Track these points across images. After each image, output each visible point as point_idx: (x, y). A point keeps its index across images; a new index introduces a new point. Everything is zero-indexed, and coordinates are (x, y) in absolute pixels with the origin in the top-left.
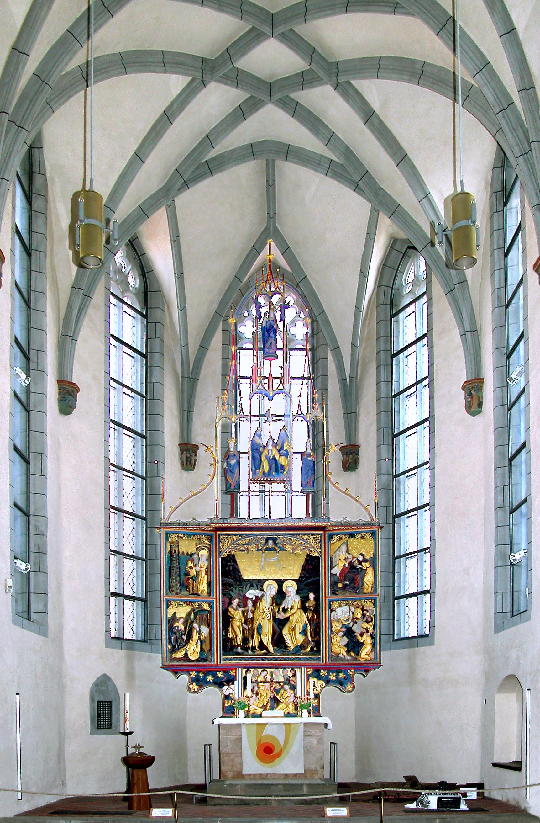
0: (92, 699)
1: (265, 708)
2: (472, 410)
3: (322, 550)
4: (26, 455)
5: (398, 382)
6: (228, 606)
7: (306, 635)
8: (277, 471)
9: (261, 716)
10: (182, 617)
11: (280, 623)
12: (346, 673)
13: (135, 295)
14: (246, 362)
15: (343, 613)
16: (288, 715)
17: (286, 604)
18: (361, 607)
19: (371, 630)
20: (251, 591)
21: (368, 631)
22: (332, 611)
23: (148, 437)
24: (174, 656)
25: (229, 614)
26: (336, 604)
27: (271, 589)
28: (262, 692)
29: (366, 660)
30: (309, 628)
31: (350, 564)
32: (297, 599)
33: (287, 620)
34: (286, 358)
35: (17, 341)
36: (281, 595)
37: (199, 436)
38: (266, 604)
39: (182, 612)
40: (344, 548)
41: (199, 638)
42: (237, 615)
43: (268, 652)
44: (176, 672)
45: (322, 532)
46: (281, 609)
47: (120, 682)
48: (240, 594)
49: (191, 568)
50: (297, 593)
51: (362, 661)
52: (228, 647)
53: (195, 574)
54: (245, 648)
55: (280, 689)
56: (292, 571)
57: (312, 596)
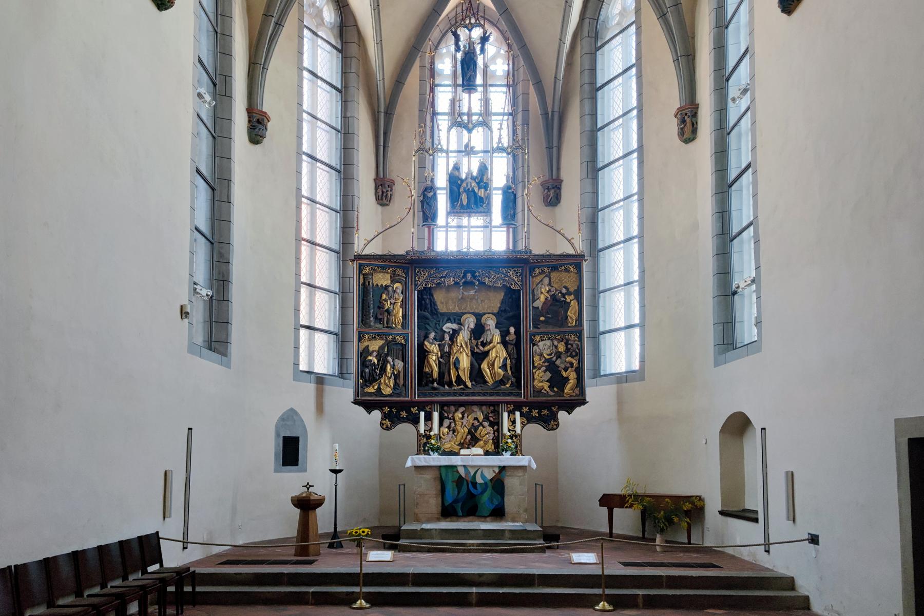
0: (277, 435)
1: (462, 445)
2: (685, 136)
4: (218, 185)
5: (603, 115)
7: (506, 370)
8: (476, 204)
9: (457, 454)
11: (478, 357)
12: (549, 410)
13: (332, 29)
14: (443, 99)
16: (487, 453)
17: (485, 338)
19: (575, 362)
20: (449, 325)
21: (572, 367)
22: (534, 345)
23: (345, 173)
24: (366, 390)
26: (538, 338)
27: (470, 322)
28: (459, 428)
30: (509, 361)
31: (553, 296)
32: (498, 332)
33: (487, 354)
34: (486, 92)
35: (200, 61)
36: (479, 331)
38: (463, 336)
39: (375, 345)
40: (546, 281)
41: (393, 373)
42: (433, 348)
43: (466, 386)
44: (369, 406)
47: (307, 413)
50: (496, 327)
51: (566, 397)
52: (424, 378)
54: (441, 382)
55: (478, 426)
56: (495, 301)
57: (512, 330)
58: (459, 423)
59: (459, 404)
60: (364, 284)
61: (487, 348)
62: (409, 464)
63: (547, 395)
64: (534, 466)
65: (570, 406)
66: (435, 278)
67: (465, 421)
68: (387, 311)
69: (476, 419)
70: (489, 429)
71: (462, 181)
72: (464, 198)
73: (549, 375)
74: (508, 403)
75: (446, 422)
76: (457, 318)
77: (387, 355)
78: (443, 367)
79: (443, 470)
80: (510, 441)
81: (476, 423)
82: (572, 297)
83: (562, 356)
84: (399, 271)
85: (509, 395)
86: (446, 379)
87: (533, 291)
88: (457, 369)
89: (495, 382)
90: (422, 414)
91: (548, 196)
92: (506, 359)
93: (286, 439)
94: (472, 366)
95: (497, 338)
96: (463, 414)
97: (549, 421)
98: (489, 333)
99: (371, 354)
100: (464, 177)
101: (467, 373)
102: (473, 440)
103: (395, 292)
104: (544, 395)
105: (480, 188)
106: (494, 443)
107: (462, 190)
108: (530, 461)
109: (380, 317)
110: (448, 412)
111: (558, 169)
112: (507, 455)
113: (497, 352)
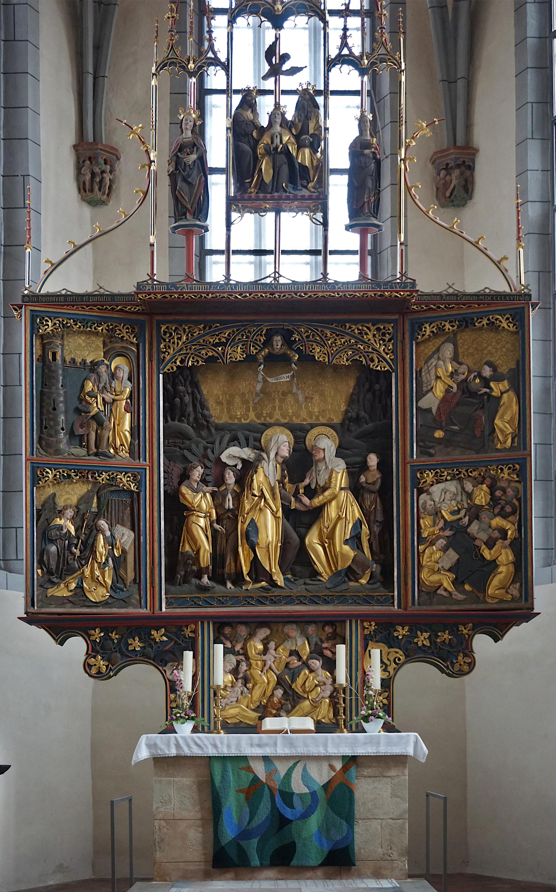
6: (180, 484)
9: (254, 729)
11: (300, 519)
12: (454, 630)
16: (320, 728)
18: (488, 481)
20: (234, 450)
24: (51, 592)
26: (429, 476)
27: (281, 443)
29: (501, 601)
30: (365, 529)
31: (464, 385)
32: (340, 466)
33: (317, 513)
36: (300, 463)
38: (267, 476)
40: (448, 350)
41: (111, 554)
43: (273, 584)
44: (60, 628)
45: (397, 317)
46: (301, 491)
48: (206, 456)
49: (92, 395)
52: (179, 566)
53: (102, 408)
56: (332, 400)
57: (373, 460)
59: (255, 623)
60: (43, 358)
61: (317, 501)
65: (499, 623)
66: (204, 345)
67: (269, 658)
73: (453, 556)
77: (97, 515)
78: (221, 541)
81: (295, 663)
82: (505, 385)
83: (484, 515)
84: (123, 332)
85: (367, 600)
86: (229, 567)
87: (419, 373)
88: (253, 547)
89: (336, 574)
91: (446, 185)
92: (358, 524)
95: (340, 479)
96: (265, 642)
97: (454, 658)
99: (61, 513)
100: (264, 121)
101: (275, 556)
103: (113, 376)
105: (300, 146)
107: (260, 150)
109: (80, 431)
111: (469, 126)
113: (339, 508)
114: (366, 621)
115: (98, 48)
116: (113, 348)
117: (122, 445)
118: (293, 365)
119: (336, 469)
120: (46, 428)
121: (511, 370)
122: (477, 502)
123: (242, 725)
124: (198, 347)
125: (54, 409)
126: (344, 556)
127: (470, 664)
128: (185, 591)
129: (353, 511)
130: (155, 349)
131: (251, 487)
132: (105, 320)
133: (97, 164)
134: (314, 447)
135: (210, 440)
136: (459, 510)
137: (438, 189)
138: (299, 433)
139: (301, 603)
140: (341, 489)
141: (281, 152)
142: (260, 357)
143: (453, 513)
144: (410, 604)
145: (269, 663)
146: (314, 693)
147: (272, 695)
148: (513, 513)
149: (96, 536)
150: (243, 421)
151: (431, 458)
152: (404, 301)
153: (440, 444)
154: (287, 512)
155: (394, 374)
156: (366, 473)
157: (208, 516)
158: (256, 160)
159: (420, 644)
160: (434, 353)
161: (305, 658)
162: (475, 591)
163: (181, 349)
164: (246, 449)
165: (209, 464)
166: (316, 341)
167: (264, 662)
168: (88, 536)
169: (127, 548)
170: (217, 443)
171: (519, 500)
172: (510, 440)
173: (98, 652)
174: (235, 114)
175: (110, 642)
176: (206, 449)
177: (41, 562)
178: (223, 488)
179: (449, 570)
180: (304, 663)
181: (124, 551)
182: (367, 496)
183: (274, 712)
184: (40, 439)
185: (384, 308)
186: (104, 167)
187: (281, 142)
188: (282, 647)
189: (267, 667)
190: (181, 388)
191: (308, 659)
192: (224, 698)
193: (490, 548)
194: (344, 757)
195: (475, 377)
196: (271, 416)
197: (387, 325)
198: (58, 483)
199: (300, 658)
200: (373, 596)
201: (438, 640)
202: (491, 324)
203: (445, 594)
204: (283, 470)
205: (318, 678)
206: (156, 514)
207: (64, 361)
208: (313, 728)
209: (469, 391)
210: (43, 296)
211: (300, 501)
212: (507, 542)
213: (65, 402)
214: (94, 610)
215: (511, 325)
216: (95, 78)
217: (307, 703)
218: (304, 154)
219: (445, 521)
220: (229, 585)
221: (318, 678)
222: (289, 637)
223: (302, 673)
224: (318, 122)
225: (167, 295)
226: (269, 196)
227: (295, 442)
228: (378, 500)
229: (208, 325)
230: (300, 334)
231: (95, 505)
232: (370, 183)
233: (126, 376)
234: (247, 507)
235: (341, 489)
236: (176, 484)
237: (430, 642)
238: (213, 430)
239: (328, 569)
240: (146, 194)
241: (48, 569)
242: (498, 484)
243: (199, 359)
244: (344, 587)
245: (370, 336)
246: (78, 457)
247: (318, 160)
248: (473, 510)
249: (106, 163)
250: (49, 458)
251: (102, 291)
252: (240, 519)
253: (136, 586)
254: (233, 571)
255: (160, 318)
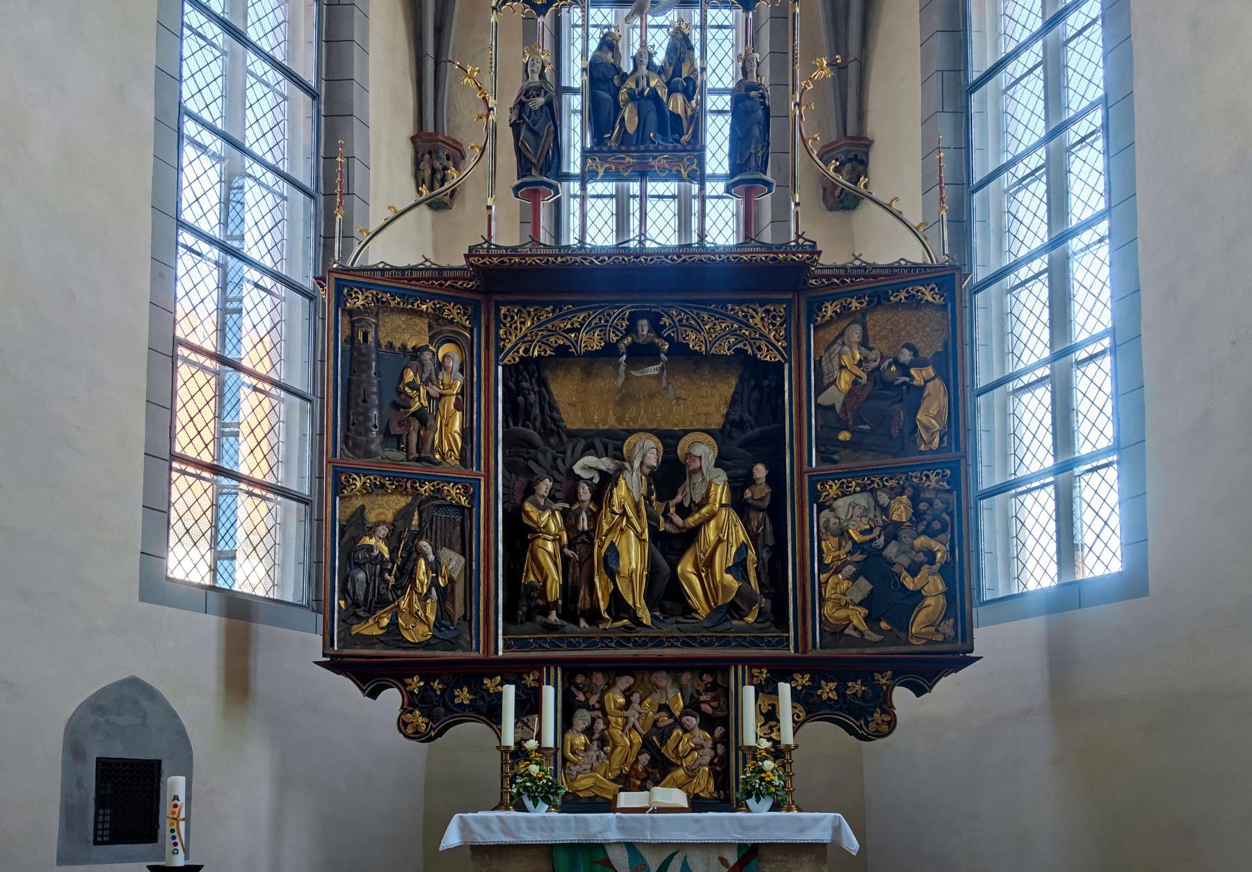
1: (627, 782)
3: (789, 344)
6: (523, 500)
9: (609, 806)
10: (384, 523)
11: (670, 545)
12: (868, 680)
15: (851, 510)
16: (697, 804)
18: (909, 491)
20: (589, 460)
23: (331, 100)
24: (356, 629)
25: (526, 521)
26: (833, 489)
27: (648, 451)
28: (617, 732)
29: (930, 642)
30: (752, 554)
31: (875, 374)
32: (721, 477)
33: (692, 536)
36: (669, 476)
37: (467, 126)
38: (629, 490)
40: (855, 333)
41: (434, 583)
42: (550, 521)
43: (637, 621)
44: (370, 676)
45: (789, 296)
46: (672, 510)
48: (555, 468)
49: (413, 386)
51: (917, 645)
52: (522, 600)
53: (426, 403)
55: (671, 728)
56: (712, 399)
57: (760, 471)
58: (616, 720)
59: (615, 669)
60: (351, 339)
61: (692, 521)
62: (452, 838)
63: (861, 641)
64: (852, 843)
65: (923, 672)
66: (553, 332)
67: (632, 715)
68: (421, 416)
69: (664, 708)
70: (701, 735)
71: (624, 77)
72: (630, 116)
73: (865, 586)
74: (754, 663)
75: (582, 718)
76: (611, 444)
77: (419, 535)
78: (575, 572)
79: (562, 859)
80: (769, 765)
81: (665, 720)
82: (930, 371)
83: (905, 534)
84: (453, 312)
85: (754, 643)
86: (583, 602)
87: (818, 363)
88: (612, 574)
89: (715, 611)
90: (509, 692)
92: (743, 548)
93: (107, 768)
94: (653, 569)
95: (720, 493)
96: (627, 694)
97: (866, 715)
98: (698, 478)
99: (371, 532)
101: (640, 587)
102: (657, 768)
103: (440, 366)
104: (852, 642)
106: (715, 774)
107: (623, 95)
108: (837, 830)
109: (396, 430)
110: (588, 691)
111: (861, 116)
112: (760, 811)
113: (719, 529)
114: (756, 667)
115: (439, 30)
116: (440, 332)
117: (451, 450)
118: (662, 356)
119: (715, 481)
120: (354, 424)
121: (937, 353)
122: (895, 517)
123: (597, 800)
124: (545, 333)
125: (365, 401)
126: (726, 588)
127: (889, 723)
128: (527, 631)
129: (737, 532)
130: (492, 336)
131: (610, 505)
132: (432, 297)
133: (438, 158)
134: (689, 455)
135: (561, 449)
136: (871, 531)
137: (824, 190)
138: (668, 440)
139: (673, 646)
140: (722, 505)
141: (648, 97)
142: (622, 347)
143: (863, 533)
144: (810, 647)
145: (632, 719)
146: (689, 758)
147: (637, 761)
148: (943, 530)
149: (416, 560)
150: (601, 427)
151: (833, 466)
152: (803, 268)
153: (845, 448)
154: (655, 535)
155: (787, 366)
156: (753, 487)
157: (557, 540)
158: (618, 109)
159: (825, 696)
160: (837, 338)
161: (677, 714)
162: (895, 630)
163: (525, 336)
164: (604, 459)
165: (559, 477)
166: (690, 326)
167: (626, 718)
168: (406, 560)
169: (455, 576)
170: (569, 452)
171: (951, 514)
172: (937, 440)
173: (415, 706)
174: (593, 57)
175: (431, 693)
176: (555, 459)
177: (344, 592)
178: (576, 506)
179: (860, 604)
180: (676, 720)
181: (451, 580)
182: (753, 514)
183: (638, 783)
184: (346, 439)
185: (775, 278)
186: (446, 163)
187: (648, 85)
188: (649, 700)
189: (629, 725)
190: (525, 384)
191: (683, 714)
192: (576, 764)
193: (914, 575)
194: (740, 846)
195: (890, 365)
196: (634, 420)
197: (777, 306)
198: (368, 493)
199: (671, 715)
200: (762, 638)
201: (848, 692)
202: (910, 297)
203: (855, 634)
204: (649, 485)
205: (695, 740)
206: (492, 536)
207: (378, 344)
208: (686, 805)
209: (882, 380)
210: (354, 270)
211: (671, 521)
212: (936, 567)
213: (380, 394)
214: (412, 653)
215: (937, 297)
216: (437, 64)
217: (681, 772)
218: (676, 100)
219: (854, 542)
220: (583, 623)
221: (695, 740)
222: (658, 687)
223: (675, 733)
224: (692, 64)
225: (506, 259)
226: (633, 148)
227: (665, 452)
228: (767, 520)
229: (558, 305)
230: (670, 317)
231: (415, 522)
232: (756, 131)
233: (457, 366)
234: (606, 527)
235: (722, 505)
236: (518, 501)
237: (838, 695)
238: (564, 437)
239: (705, 605)
240: (483, 150)
241: (353, 600)
242: (922, 495)
243: (547, 348)
244: (727, 626)
245: (758, 320)
246: (394, 462)
247: (693, 110)
248: (890, 527)
249: (448, 159)
250: (357, 462)
251: (428, 264)
252: (597, 542)
253: (467, 624)
254: (588, 606)
255: (499, 298)
